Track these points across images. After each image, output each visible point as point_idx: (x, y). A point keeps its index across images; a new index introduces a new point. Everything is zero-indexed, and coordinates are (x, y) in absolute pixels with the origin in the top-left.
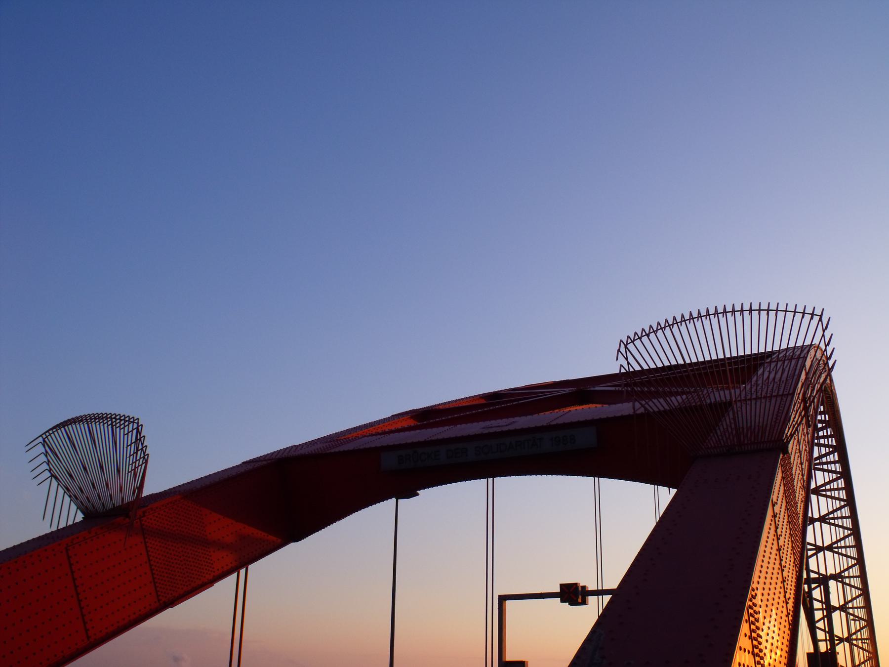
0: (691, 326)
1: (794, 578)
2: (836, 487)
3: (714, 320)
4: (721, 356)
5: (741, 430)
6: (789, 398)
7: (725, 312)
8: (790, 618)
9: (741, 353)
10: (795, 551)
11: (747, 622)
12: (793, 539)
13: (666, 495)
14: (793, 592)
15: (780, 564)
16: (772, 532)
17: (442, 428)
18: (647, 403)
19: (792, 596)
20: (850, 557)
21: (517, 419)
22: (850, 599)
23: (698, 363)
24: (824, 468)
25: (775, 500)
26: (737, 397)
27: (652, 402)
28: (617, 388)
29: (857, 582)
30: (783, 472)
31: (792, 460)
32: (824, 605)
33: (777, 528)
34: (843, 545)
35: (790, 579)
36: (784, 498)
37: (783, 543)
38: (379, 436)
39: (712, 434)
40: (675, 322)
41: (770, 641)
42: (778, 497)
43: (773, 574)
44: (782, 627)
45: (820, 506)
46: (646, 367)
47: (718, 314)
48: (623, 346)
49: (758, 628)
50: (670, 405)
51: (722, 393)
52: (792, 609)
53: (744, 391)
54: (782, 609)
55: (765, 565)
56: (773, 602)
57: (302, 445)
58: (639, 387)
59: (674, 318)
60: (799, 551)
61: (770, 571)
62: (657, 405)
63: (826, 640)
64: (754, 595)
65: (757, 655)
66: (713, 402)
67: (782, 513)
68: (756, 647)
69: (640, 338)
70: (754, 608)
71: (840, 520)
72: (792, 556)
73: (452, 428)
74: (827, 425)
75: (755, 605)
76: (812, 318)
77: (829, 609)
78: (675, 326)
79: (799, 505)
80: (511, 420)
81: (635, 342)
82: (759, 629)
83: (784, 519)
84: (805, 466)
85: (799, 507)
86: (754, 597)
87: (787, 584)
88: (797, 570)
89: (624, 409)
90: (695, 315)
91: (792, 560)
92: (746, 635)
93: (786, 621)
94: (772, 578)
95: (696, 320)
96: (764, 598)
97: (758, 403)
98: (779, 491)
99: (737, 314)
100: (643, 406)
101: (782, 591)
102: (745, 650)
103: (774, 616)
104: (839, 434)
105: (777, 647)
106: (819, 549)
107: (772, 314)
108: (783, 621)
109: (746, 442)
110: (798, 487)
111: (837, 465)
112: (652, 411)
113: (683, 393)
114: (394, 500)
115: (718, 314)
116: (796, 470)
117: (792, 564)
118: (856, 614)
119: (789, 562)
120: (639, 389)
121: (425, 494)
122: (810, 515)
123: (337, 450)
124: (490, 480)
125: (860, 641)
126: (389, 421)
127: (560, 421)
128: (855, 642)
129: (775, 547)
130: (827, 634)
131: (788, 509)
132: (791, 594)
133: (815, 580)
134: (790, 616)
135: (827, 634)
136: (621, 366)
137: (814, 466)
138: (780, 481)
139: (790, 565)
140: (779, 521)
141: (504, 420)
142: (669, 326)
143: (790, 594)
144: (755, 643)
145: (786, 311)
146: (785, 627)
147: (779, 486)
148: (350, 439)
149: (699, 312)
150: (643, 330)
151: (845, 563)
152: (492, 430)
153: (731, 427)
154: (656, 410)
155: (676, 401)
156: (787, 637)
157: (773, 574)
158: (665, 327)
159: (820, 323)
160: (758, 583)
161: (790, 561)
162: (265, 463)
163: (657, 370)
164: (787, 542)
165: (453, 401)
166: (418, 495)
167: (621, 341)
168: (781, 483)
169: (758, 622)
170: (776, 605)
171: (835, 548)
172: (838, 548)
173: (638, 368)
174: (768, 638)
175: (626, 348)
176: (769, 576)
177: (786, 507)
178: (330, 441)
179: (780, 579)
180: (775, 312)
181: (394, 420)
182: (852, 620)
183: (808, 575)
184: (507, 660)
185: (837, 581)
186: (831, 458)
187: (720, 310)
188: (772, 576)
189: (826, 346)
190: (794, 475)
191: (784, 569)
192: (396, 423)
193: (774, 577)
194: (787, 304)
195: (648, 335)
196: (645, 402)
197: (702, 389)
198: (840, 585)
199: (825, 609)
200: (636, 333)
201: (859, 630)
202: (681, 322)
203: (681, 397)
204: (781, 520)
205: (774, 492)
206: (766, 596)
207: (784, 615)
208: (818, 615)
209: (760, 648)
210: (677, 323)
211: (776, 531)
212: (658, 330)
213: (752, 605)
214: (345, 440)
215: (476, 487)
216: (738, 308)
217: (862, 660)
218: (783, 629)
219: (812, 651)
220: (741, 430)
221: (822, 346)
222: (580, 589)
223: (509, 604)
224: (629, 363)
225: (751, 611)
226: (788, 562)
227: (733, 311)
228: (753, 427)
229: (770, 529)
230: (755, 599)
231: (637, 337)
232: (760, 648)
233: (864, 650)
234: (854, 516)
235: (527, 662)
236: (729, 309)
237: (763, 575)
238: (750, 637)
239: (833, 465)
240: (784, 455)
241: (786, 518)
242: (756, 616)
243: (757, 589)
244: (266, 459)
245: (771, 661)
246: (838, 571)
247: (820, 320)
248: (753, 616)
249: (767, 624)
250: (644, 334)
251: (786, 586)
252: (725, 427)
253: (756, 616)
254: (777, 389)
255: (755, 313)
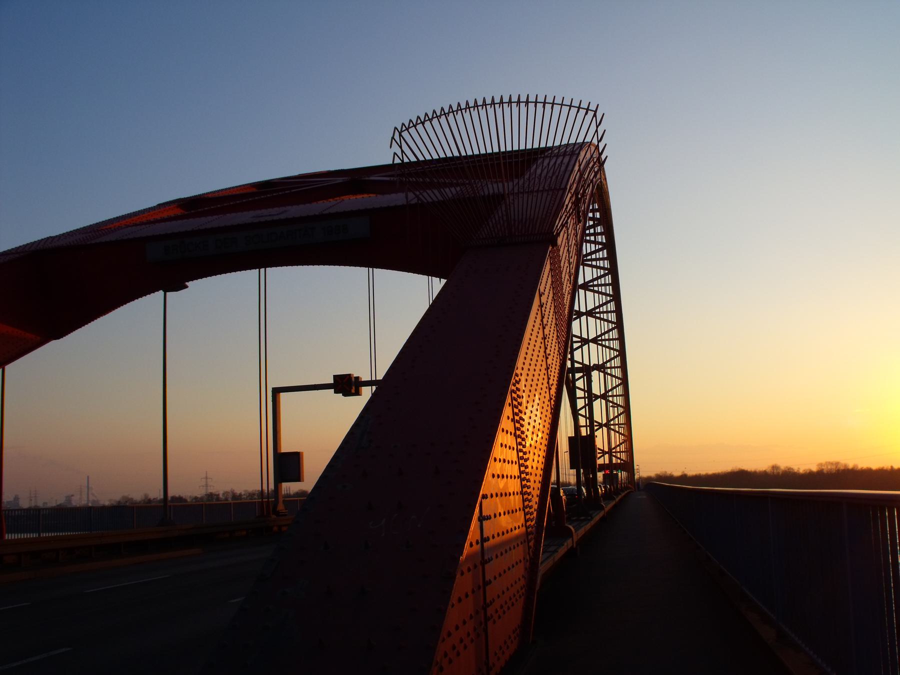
0: (467, 115)
1: (557, 369)
2: (603, 283)
3: (491, 111)
4: (496, 150)
5: (512, 222)
6: (561, 192)
7: (502, 102)
8: (553, 403)
9: (516, 148)
10: (559, 340)
11: (510, 406)
12: (558, 329)
13: (438, 284)
14: (556, 379)
15: (545, 352)
16: (538, 321)
17: (210, 217)
18: (421, 194)
19: (555, 382)
20: (613, 349)
21: (289, 208)
22: (610, 388)
23: (473, 156)
24: (593, 264)
25: (542, 290)
26: (510, 190)
27: (427, 192)
28: (392, 178)
29: (618, 372)
30: (551, 264)
31: (561, 253)
32: (586, 394)
33: (543, 317)
34: (607, 338)
35: (554, 366)
36: (551, 289)
37: (548, 332)
38: (144, 226)
39: (484, 226)
40: (451, 111)
41: (532, 423)
42: (545, 288)
43: (537, 361)
44: (544, 411)
45: (586, 300)
46: (421, 158)
47: (486, 105)
48: (397, 134)
49: (520, 411)
50: (444, 196)
51: (495, 186)
52: (554, 395)
53: (517, 186)
54: (545, 395)
55: (530, 352)
56: (541, 391)
57: (59, 237)
58: (414, 177)
59: (451, 107)
60: (564, 341)
61: (535, 358)
62: (432, 195)
63: (586, 426)
64: (518, 380)
65: (519, 436)
66: (491, 194)
67: (549, 304)
68: (519, 429)
69: (415, 126)
70: (518, 393)
71: (605, 315)
72: (557, 345)
73: (221, 217)
74: (597, 222)
75: (518, 389)
76: (586, 113)
77: (591, 397)
78: (451, 114)
79: (566, 296)
80: (282, 209)
81: (410, 130)
82: (521, 412)
83: (550, 309)
84: (573, 260)
85: (565, 299)
86: (518, 382)
87: (551, 371)
88: (561, 358)
89: (397, 199)
90: (472, 104)
91: (557, 349)
92: (508, 418)
93: (548, 406)
94: (536, 365)
95: (472, 109)
96: (528, 384)
97: (530, 197)
98: (547, 282)
99: (514, 105)
100: (417, 196)
101: (546, 377)
102: (507, 432)
103: (537, 401)
104: (609, 232)
105: (539, 430)
106: (585, 342)
107: (548, 107)
108: (545, 406)
109: (517, 234)
110: (566, 279)
111: (606, 261)
112: (425, 201)
113: (457, 185)
114: (161, 293)
115: (503, 103)
116: (564, 263)
117: (556, 352)
118: (615, 402)
119: (553, 354)
120: (415, 180)
121: (195, 286)
122: (576, 308)
123: (98, 241)
124: (262, 270)
125: (617, 426)
126: (155, 210)
127: (333, 211)
128: (612, 427)
129: (541, 335)
130: (588, 420)
131: (555, 300)
132: (554, 381)
133: (579, 370)
134: (552, 401)
135: (588, 420)
136: (395, 154)
137: (583, 258)
138: (548, 272)
139: (554, 353)
140: (545, 311)
141: (276, 209)
142: (445, 114)
143: (553, 380)
144: (518, 425)
145: (562, 105)
146: (547, 411)
147: (547, 277)
148: (113, 229)
149: (476, 101)
150: (418, 117)
151: (608, 354)
152: (262, 220)
153: (503, 219)
154: (430, 200)
155: (450, 192)
156: (548, 421)
157: (537, 361)
158: (433, 118)
159: (594, 118)
160: (523, 369)
161: (555, 349)
162: (17, 255)
163: (432, 161)
164: (552, 331)
165: (222, 190)
166: (186, 287)
167: (396, 128)
168: (549, 274)
169: (521, 406)
170: (539, 390)
171: (600, 340)
172: (602, 340)
173: (413, 159)
174: (530, 421)
175: (400, 135)
176: (533, 363)
177: (553, 297)
178: (91, 232)
179: (544, 366)
180: (551, 105)
181: (160, 208)
182: (611, 406)
183: (572, 364)
184: (282, 452)
185: (600, 371)
186: (600, 255)
187: (497, 100)
188: (537, 363)
189: (598, 142)
190: (562, 268)
191: (549, 357)
192: (172, 210)
193: (538, 364)
194: (563, 98)
195: (423, 123)
196: (420, 192)
197: (482, 181)
198: (602, 374)
199: (587, 398)
200: (411, 121)
201: (617, 417)
202: (457, 111)
203: (455, 189)
204: (548, 310)
205: (541, 282)
206: (530, 382)
207: (546, 400)
208: (580, 403)
209: (522, 430)
210: (453, 112)
211: (542, 320)
212: (433, 118)
213: (515, 389)
214: (106, 231)
215: (251, 275)
216: (523, 99)
217: (614, 385)
218: (545, 413)
219: (333, 390)
220: (512, 222)
221: (595, 141)
222: (353, 379)
223: (283, 396)
224: (402, 151)
225: (514, 395)
226: (553, 351)
227: (519, 102)
228: (524, 220)
229: (536, 318)
230: (518, 384)
231: (411, 125)
232: (522, 430)
233: (620, 434)
234: (618, 311)
235: (302, 453)
236: (506, 99)
237: (527, 362)
238: (513, 420)
239: (601, 262)
240: (553, 248)
241: (552, 308)
242: (519, 400)
243: (521, 374)
244: (19, 251)
245: (533, 443)
246: (601, 363)
247: (595, 115)
248: (516, 400)
249: (530, 408)
250: (419, 121)
251: (549, 373)
252: (497, 219)
253: (519, 400)
254: (555, 182)
255: (531, 106)
